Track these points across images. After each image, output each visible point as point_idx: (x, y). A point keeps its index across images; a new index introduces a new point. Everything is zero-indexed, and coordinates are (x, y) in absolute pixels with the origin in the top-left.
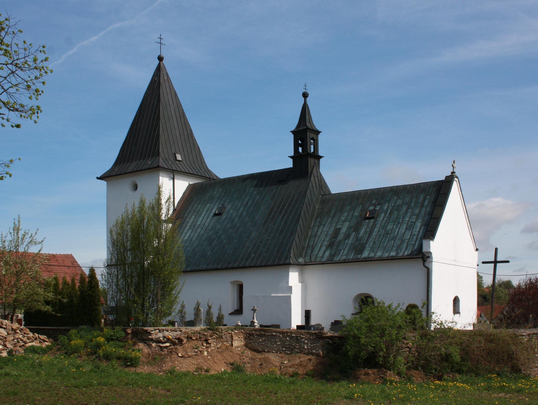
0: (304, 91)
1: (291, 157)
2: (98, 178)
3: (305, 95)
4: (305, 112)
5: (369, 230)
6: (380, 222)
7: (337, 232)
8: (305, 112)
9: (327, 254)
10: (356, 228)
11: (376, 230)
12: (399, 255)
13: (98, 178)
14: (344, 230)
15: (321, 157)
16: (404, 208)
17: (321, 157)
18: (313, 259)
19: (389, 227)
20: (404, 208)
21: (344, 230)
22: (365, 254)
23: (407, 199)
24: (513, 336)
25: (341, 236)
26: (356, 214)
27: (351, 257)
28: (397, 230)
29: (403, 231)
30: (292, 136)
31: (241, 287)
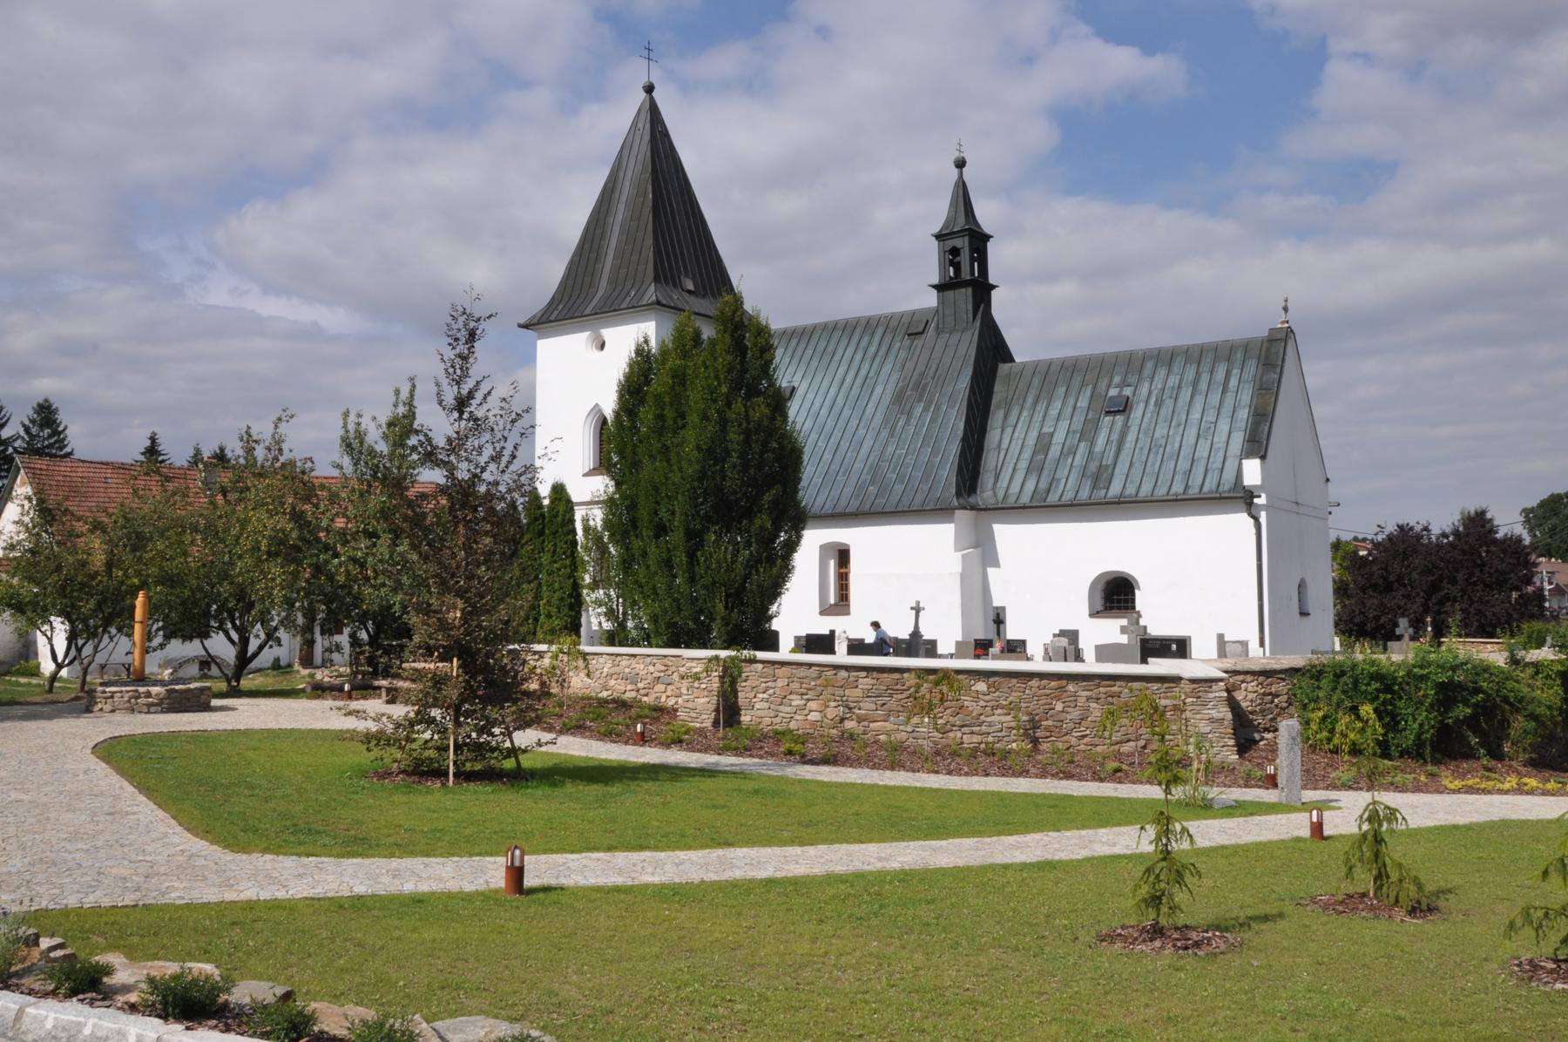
0: (957, 154)
1: (934, 287)
2: (520, 326)
3: (961, 164)
4: (963, 198)
5: (1115, 437)
6: (1137, 422)
7: (1044, 444)
8: (963, 198)
9: (1030, 486)
10: (1088, 432)
11: (1131, 437)
12: (1127, 492)
13: (520, 326)
14: (1059, 438)
15: (994, 287)
16: (1186, 394)
17: (994, 287)
18: (1196, 480)
19: (1161, 432)
20: (1186, 394)
21: (1059, 438)
22: (1115, 489)
23: (1190, 374)
24: (1064, 642)
25: (1055, 451)
26: (1083, 403)
27: (1084, 494)
28: (1178, 439)
29: (1192, 440)
30: (987, 229)
31: (843, 556)
